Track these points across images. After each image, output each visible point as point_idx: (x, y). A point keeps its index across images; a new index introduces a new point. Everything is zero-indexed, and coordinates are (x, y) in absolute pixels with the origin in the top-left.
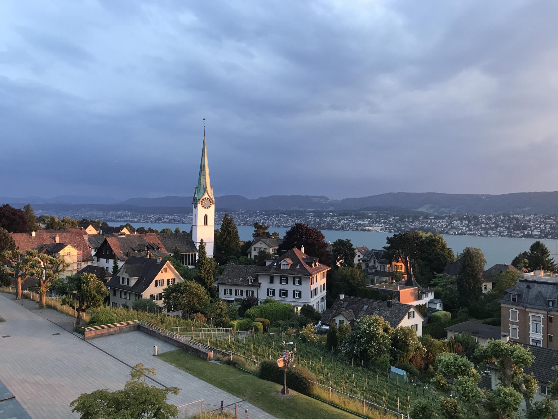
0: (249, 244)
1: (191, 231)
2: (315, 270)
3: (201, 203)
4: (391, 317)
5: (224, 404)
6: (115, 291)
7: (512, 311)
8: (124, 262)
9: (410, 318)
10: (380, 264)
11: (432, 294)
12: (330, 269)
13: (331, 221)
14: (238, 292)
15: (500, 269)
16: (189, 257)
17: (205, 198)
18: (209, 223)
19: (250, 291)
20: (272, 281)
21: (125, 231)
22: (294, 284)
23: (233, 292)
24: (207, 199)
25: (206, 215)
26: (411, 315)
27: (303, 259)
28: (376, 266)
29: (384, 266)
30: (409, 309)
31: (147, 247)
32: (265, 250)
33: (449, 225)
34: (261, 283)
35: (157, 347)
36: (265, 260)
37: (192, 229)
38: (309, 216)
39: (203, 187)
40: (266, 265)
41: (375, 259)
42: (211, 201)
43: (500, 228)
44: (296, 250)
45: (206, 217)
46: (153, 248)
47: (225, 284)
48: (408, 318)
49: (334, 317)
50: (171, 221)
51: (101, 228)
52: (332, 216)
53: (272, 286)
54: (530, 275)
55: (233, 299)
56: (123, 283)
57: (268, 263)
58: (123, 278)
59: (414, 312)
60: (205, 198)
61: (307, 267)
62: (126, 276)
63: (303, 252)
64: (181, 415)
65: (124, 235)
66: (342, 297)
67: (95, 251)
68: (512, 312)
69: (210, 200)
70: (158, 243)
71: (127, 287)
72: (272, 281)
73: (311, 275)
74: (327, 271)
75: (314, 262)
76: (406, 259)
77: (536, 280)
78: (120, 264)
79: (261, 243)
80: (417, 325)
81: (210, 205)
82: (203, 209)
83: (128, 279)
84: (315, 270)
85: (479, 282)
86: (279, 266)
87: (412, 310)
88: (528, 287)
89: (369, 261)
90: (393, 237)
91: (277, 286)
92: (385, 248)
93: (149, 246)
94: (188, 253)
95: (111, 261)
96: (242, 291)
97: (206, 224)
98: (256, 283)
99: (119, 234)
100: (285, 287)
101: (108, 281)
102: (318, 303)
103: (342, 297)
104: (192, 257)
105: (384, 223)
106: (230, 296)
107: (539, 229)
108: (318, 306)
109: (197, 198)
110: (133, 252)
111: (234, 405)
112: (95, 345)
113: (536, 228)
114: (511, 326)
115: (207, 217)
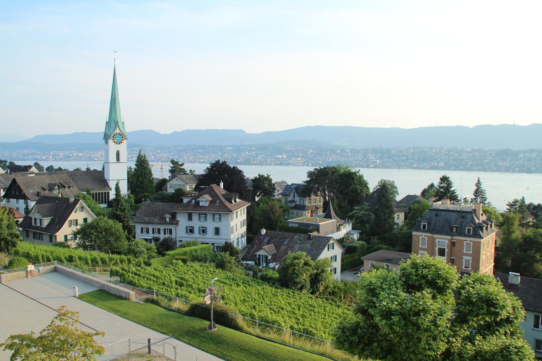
0: (164, 182)
1: (103, 169)
2: (235, 206)
3: (112, 139)
4: (312, 250)
5: (151, 341)
6: (27, 232)
7: (466, 243)
8: (35, 202)
9: (330, 250)
10: (300, 198)
11: (349, 226)
12: (250, 204)
13: (249, 155)
14: (167, 231)
15: (409, 198)
16: (99, 196)
17: (117, 133)
18: (121, 159)
19: (167, 229)
20: (190, 219)
21: (34, 169)
22: (214, 220)
23: (151, 231)
24: (118, 134)
25: (118, 151)
26: (331, 246)
27: (223, 195)
28: (296, 200)
29: (304, 200)
30: (328, 241)
31: (58, 186)
32: (182, 187)
33: (364, 158)
34: (179, 221)
35: (77, 288)
36: (182, 198)
37: (104, 166)
38: (226, 151)
39: (114, 121)
40: (184, 202)
41: (294, 193)
42: (123, 136)
43: (410, 161)
44: (214, 186)
45: (118, 154)
46: (64, 187)
47: (142, 223)
48: (328, 250)
49: (256, 252)
50: (80, 159)
51: (9, 167)
52: (249, 151)
53: (191, 224)
54: (439, 205)
55: (151, 238)
56: (35, 223)
57: (186, 200)
58: (35, 219)
59: (333, 244)
60: (117, 133)
61: (227, 204)
62: (38, 216)
63: (222, 188)
64: (107, 354)
65: (33, 174)
66: (264, 231)
67: (4, 191)
68: (466, 245)
69: (121, 135)
70: (70, 182)
71: (40, 228)
72: (190, 219)
73: (231, 211)
74: (247, 207)
75: (233, 198)
76: (324, 192)
77: (440, 208)
78: (32, 204)
79: (177, 180)
80: (336, 256)
81: (122, 141)
82: (114, 144)
83: (41, 220)
84: (235, 206)
85: (391, 213)
86: (197, 203)
87: (331, 242)
88: (436, 215)
89: (289, 195)
90: (313, 170)
91: (196, 223)
92: (307, 182)
93: (60, 185)
94: (101, 192)
95: (22, 201)
96: (159, 230)
97: (119, 161)
98: (174, 221)
99: (28, 173)
100: (204, 224)
101: (19, 223)
102: (238, 239)
103: (264, 231)
104: (105, 196)
105: (302, 156)
106: (148, 235)
107: (443, 161)
108: (238, 242)
109: (108, 134)
110: (44, 191)
111: (162, 342)
112: (7, 287)
113: (441, 160)
114: (465, 258)
115: (119, 153)
